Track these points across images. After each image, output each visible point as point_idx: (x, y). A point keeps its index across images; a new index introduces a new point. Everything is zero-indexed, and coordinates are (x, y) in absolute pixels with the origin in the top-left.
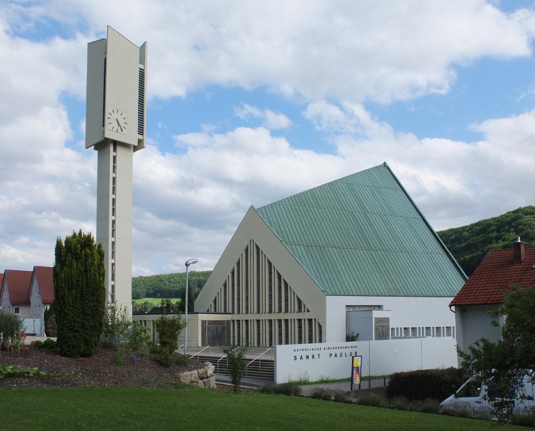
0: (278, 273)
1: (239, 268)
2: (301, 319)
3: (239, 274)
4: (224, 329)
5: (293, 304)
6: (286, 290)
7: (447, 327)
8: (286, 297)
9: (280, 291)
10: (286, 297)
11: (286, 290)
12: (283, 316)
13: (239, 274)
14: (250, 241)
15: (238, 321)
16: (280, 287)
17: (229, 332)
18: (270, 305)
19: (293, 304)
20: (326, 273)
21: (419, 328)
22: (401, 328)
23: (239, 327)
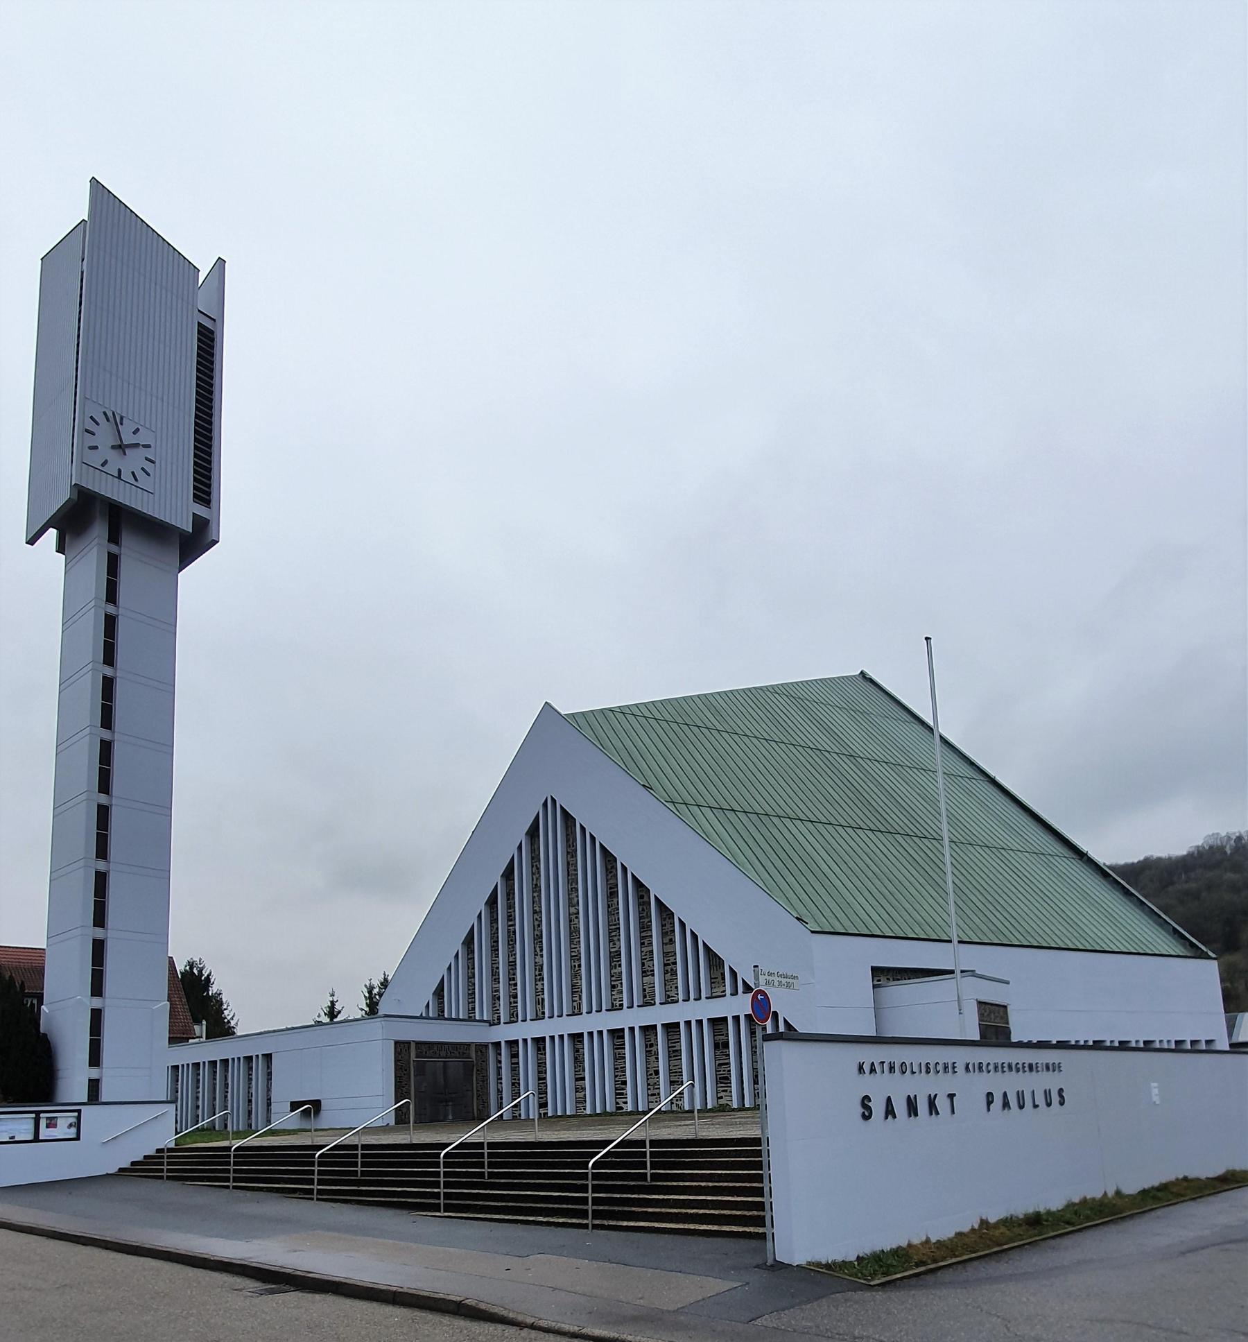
0: (638, 884)
1: (510, 894)
2: (499, 1043)
3: (510, 906)
4: (468, 1068)
5: (691, 969)
6: (667, 934)
7: (711, 1021)
8: (668, 955)
9: (645, 941)
10: (668, 955)
11: (667, 934)
12: (659, 1015)
13: (510, 906)
14: (545, 804)
15: (513, 1044)
16: (644, 927)
17: (485, 1080)
18: (508, 894)
19: (691, 969)
20: (790, 879)
21: (688, 1023)
22: (700, 1022)
23: (514, 1067)
